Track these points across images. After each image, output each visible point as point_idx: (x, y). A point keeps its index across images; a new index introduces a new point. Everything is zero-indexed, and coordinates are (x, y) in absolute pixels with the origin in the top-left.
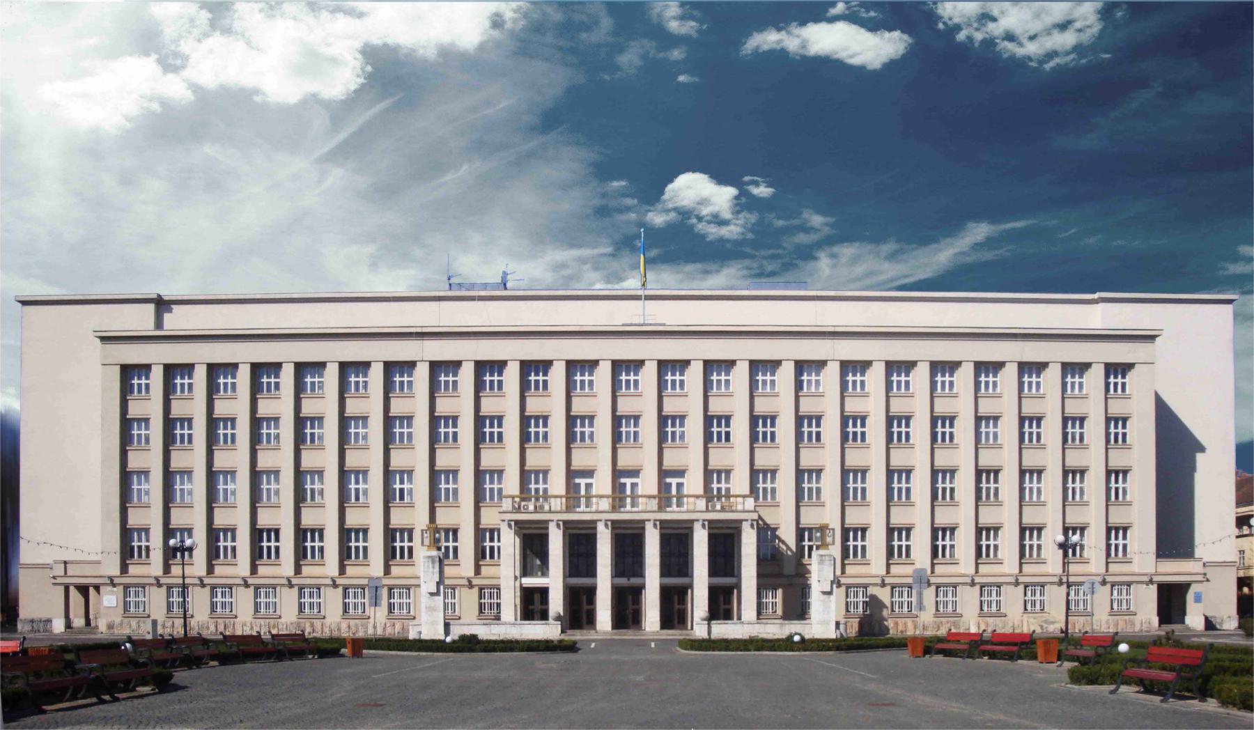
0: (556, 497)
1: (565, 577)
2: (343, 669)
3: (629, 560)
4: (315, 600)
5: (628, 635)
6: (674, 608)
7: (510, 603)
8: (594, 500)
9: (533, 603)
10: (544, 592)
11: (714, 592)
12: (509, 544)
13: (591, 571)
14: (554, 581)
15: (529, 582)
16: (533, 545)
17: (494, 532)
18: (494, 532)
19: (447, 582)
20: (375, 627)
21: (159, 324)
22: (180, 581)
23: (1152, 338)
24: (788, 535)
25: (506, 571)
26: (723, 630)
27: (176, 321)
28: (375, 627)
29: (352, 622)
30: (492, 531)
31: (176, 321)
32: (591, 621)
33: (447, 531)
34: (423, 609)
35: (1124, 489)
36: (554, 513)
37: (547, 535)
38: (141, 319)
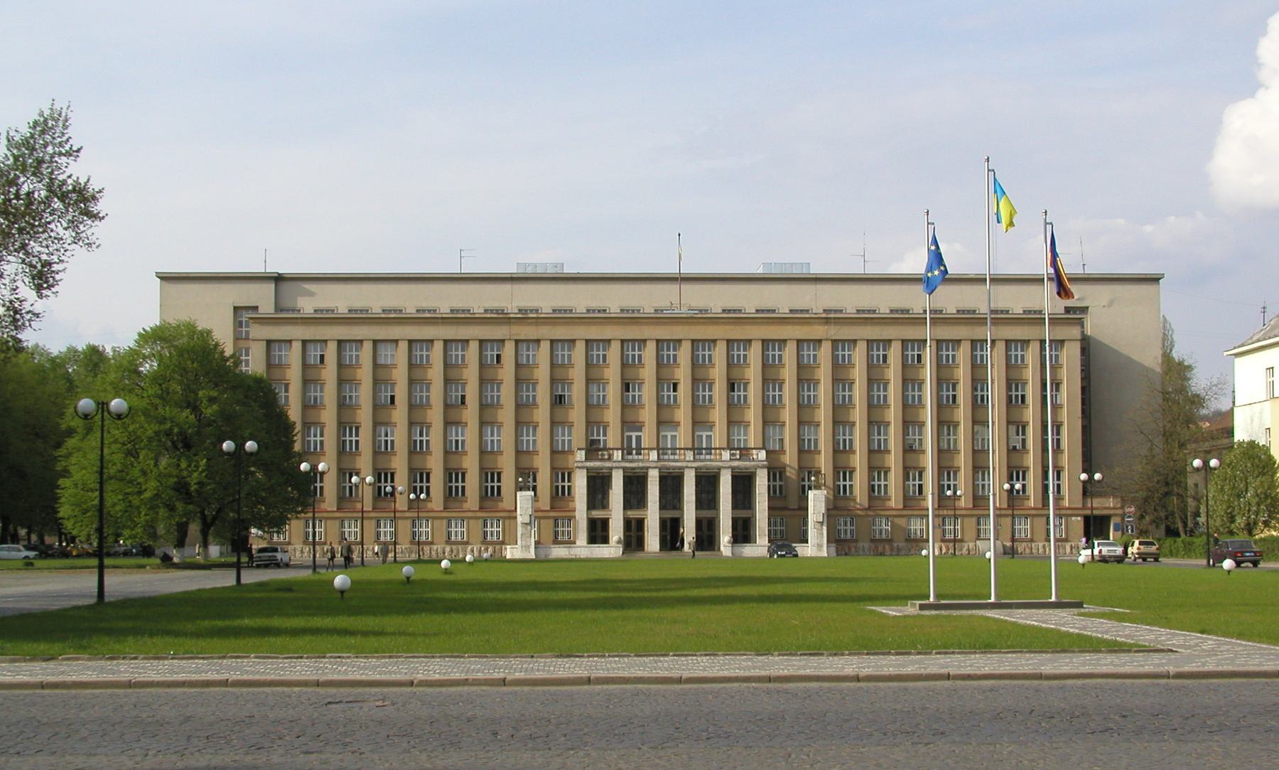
3: (670, 497)
6: (707, 539)
9: (598, 532)
13: (604, 505)
23: (1154, 280)
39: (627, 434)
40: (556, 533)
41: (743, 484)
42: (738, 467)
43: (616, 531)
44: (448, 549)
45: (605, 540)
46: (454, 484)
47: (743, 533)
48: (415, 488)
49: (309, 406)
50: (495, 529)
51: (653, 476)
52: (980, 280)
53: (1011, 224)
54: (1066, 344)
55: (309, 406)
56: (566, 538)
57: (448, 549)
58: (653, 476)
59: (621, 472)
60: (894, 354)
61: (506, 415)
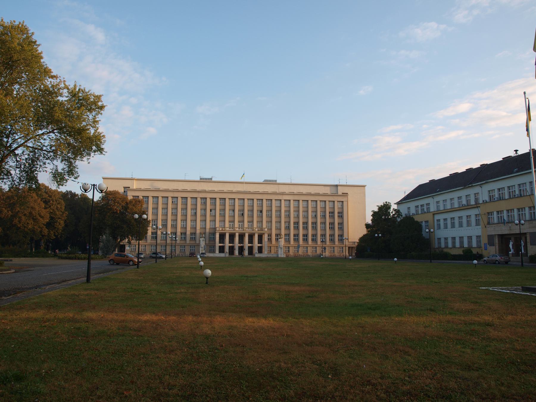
23: (364, 186)
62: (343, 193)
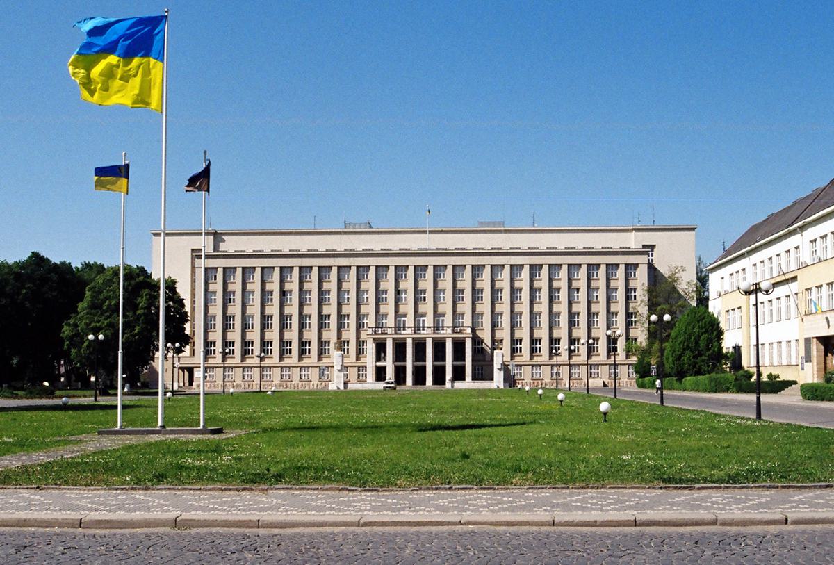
0: (448, 327)
1: (413, 362)
2: (135, 410)
4: (364, 373)
5: (419, 388)
6: (439, 378)
7: (370, 373)
8: (426, 329)
9: (380, 374)
10: (385, 368)
11: (455, 368)
12: (370, 348)
14: (389, 364)
15: (379, 364)
16: (380, 348)
17: (596, 340)
18: (596, 340)
19: (345, 365)
20: (313, 385)
21: (216, 248)
22: (613, 363)
24: (488, 341)
25: (369, 359)
26: (459, 385)
27: (229, 245)
28: (313, 385)
29: (304, 383)
30: (363, 342)
31: (229, 245)
32: (404, 382)
33: (344, 342)
34: (335, 377)
35: (348, 323)
36: (408, 334)
37: (386, 343)
38: (206, 244)
39: (437, 318)
40: (301, 376)
41: (459, 347)
42: (416, 338)
43: (390, 374)
44: (300, 384)
45: (464, 379)
46: (361, 347)
47: (459, 374)
48: (264, 350)
49: (193, 310)
50: (538, 371)
51: (409, 343)
52: (431, 232)
53: (187, 191)
54: (640, 265)
55: (193, 310)
56: (306, 378)
57: (300, 384)
58: (409, 343)
59: (391, 340)
60: (487, 273)
61: (583, 320)
62: (644, 246)
